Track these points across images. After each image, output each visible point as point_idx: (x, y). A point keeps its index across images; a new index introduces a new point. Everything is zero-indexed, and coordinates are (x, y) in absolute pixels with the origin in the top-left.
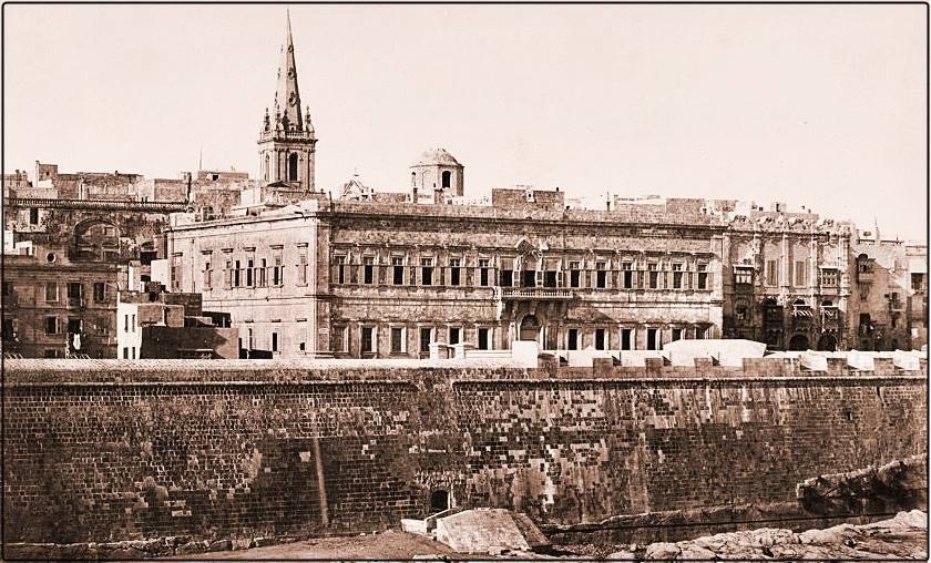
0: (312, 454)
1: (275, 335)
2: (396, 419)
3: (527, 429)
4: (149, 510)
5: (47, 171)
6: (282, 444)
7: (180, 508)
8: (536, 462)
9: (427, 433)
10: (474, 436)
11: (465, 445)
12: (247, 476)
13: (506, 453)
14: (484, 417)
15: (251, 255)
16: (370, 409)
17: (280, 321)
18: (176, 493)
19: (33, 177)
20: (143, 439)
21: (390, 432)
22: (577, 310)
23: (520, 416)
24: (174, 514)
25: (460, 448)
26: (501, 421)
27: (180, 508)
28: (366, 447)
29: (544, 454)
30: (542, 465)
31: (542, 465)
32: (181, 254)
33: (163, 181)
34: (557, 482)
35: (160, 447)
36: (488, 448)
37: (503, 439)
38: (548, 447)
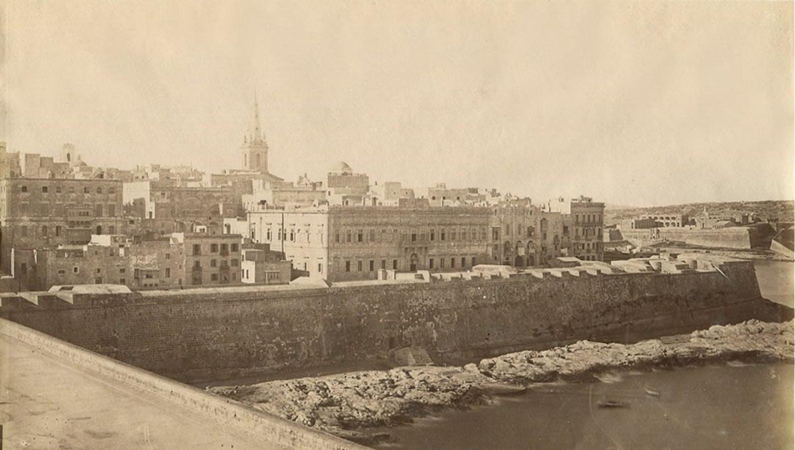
0: (342, 325)
1: (306, 264)
2: (374, 307)
3: (426, 310)
4: (279, 352)
5: (155, 168)
6: (330, 320)
7: (290, 351)
8: (429, 324)
9: (387, 313)
10: (406, 314)
11: (402, 318)
12: (316, 335)
13: (417, 320)
14: (409, 304)
15: (292, 227)
16: (364, 303)
17: (308, 258)
18: (289, 344)
19: (148, 170)
20: (275, 321)
21: (372, 313)
22: (434, 251)
23: (423, 304)
24: (288, 353)
25: (399, 319)
26: (416, 306)
27: (290, 351)
28: (363, 320)
29: (433, 320)
30: (432, 325)
31: (432, 325)
32: (255, 224)
33: (216, 175)
34: (437, 331)
35: (281, 323)
36: (411, 318)
37: (416, 314)
38: (434, 317)
